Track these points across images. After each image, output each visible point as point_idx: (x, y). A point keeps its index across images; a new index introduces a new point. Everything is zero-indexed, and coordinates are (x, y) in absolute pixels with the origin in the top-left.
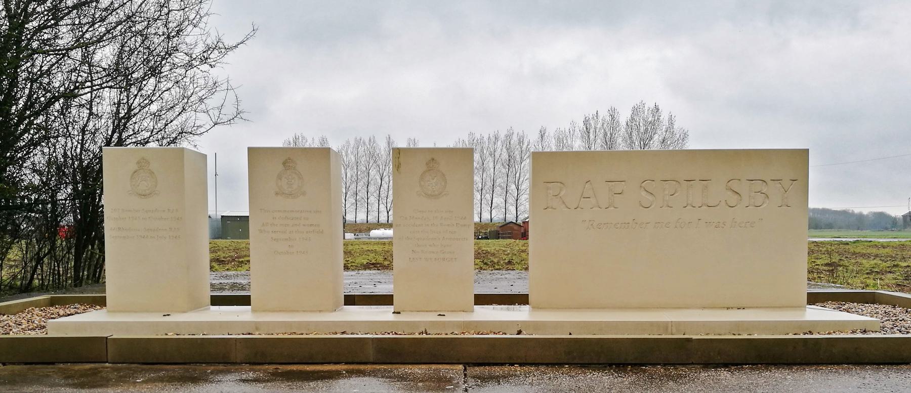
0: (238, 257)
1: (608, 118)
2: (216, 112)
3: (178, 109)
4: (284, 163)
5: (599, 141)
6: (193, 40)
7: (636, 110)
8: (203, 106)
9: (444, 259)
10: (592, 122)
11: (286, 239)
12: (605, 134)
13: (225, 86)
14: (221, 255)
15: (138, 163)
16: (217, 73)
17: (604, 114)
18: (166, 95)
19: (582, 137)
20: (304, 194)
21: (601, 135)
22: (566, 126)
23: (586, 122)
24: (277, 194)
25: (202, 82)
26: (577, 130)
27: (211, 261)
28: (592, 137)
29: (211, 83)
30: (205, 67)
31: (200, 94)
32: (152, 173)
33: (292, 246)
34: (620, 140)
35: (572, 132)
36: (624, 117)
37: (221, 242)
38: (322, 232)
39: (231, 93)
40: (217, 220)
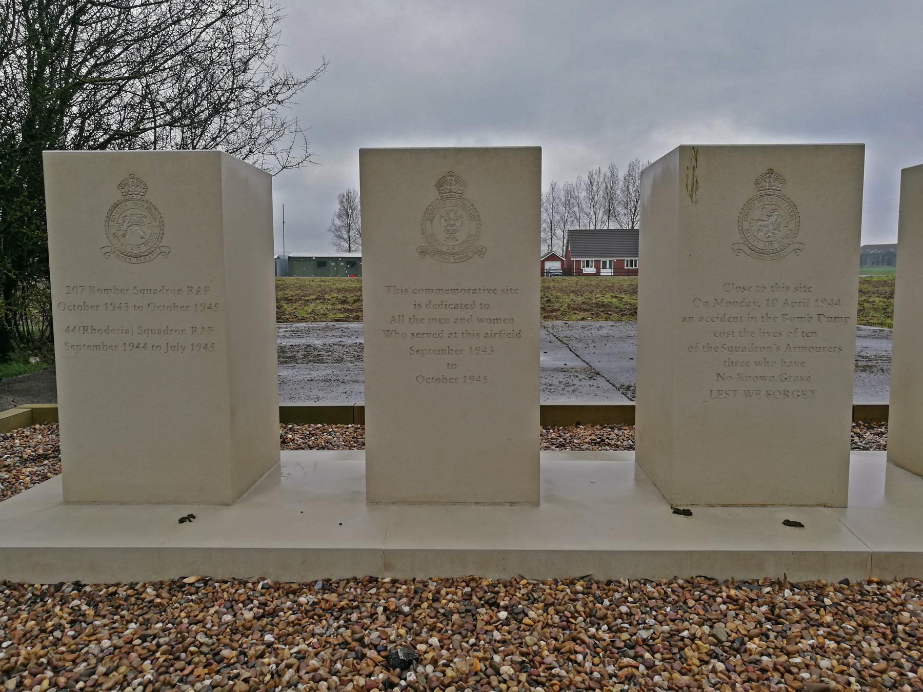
0: (305, 296)
1: (609, 174)
2: (285, 156)
3: (245, 150)
4: (439, 185)
5: (601, 192)
6: (259, 74)
7: (632, 167)
8: (270, 149)
9: (786, 393)
10: (596, 177)
11: (442, 351)
12: (607, 188)
13: (293, 128)
14: (289, 293)
15: (121, 186)
16: (284, 113)
17: (605, 170)
18: (232, 137)
19: (587, 189)
20: (481, 252)
21: (603, 187)
22: (573, 181)
23: (590, 177)
24: (423, 252)
25: (269, 123)
26: (583, 184)
27: (278, 301)
28: (595, 189)
29: (279, 124)
30: (274, 106)
31: (268, 136)
32: (152, 208)
33: (454, 366)
34: (618, 192)
35: (578, 186)
36: (621, 174)
37: (289, 280)
38: (519, 335)
39: (300, 135)
40: (284, 260)
